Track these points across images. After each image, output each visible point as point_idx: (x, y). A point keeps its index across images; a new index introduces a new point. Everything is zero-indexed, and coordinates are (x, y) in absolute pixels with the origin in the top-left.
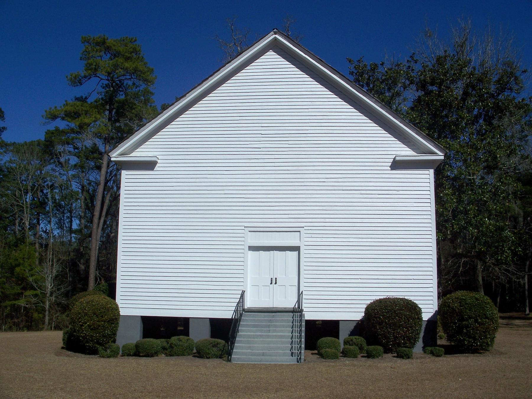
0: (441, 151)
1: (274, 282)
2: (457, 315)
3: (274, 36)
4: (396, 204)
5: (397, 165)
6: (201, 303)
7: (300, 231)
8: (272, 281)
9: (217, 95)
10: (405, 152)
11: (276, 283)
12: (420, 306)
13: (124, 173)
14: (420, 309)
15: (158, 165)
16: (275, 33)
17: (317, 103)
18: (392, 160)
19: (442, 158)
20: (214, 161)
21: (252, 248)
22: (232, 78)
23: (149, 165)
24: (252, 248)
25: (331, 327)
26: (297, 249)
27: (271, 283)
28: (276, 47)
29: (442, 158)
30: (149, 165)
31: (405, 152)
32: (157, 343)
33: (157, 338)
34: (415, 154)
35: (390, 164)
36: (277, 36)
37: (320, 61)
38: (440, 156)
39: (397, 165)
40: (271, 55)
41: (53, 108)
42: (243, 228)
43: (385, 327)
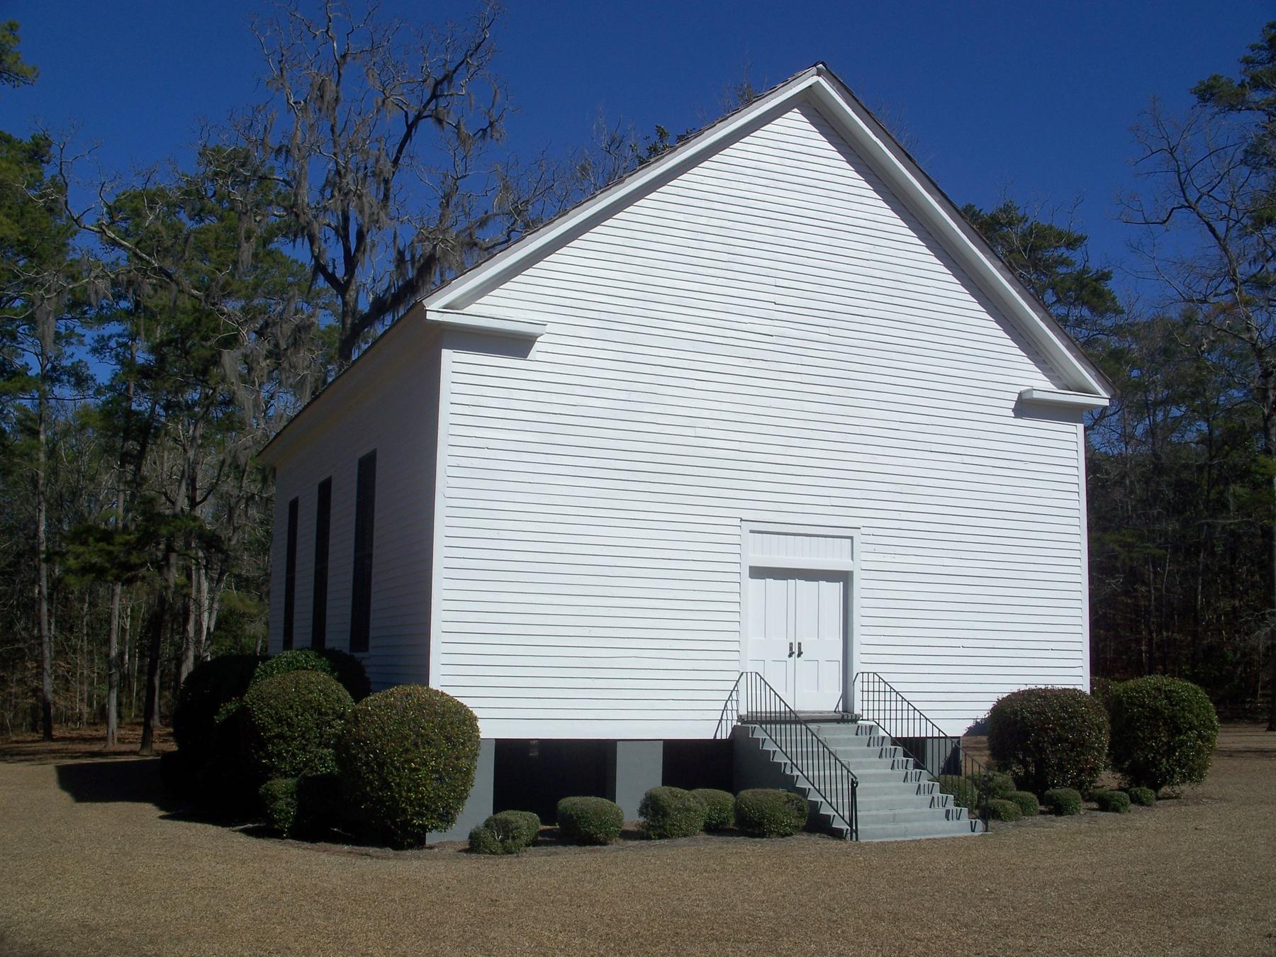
0: (1106, 390)
1: (796, 650)
2: (1164, 724)
3: (816, 79)
4: (1022, 491)
5: (1027, 407)
6: (651, 700)
7: (851, 538)
8: (791, 648)
9: (681, 191)
10: (1041, 385)
11: (799, 655)
12: (476, 713)
13: (448, 356)
14: (476, 719)
15: (537, 346)
16: (819, 75)
17: (884, 251)
18: (1015, 397)
19: (1106, 403)
20: (672, 353)
21: (758, 573)
22: (714, 158)
23: (515, 344)
24: (758, 573)
25: (589, 764)
26: (844, 578)
27: (790, 656)
28: (811, 105)
29: (1106, 403)
30: (515, 344)
31: (1041, 385)
32: (702, 800)
33: (689, 787)
34: (1052, 387)
35: (1012, 405)
36: (821, 80)
37: (907, 157)
38: (1101, 398)
39: (1027, 407)
40: (795, 117)
41: (1020, 213)
42: (737, 522)
43: (1023, 755)
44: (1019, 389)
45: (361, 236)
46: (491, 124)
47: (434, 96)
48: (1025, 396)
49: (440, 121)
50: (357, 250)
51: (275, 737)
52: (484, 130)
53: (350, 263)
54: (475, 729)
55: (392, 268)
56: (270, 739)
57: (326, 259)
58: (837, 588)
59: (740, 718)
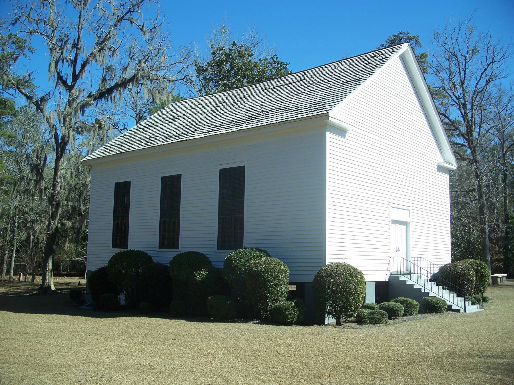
21: (395, 222)
24: (395, 222)
29: (456, 168)
38: (454, 166)
44: (438, 162)
45: (83, 66)
46: (155, 27)
47: (130, 11)
48: (440, 165)
49: (132, 22)
50: (81, 71)
51: (274, 284)
52: (151, 30)
53: (75, 77)
54: (363, 277)
55: (100, 82)
56: (271, 286)
57: (63, 74)
58: (404, 227)
59: (391, 274)
